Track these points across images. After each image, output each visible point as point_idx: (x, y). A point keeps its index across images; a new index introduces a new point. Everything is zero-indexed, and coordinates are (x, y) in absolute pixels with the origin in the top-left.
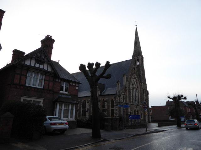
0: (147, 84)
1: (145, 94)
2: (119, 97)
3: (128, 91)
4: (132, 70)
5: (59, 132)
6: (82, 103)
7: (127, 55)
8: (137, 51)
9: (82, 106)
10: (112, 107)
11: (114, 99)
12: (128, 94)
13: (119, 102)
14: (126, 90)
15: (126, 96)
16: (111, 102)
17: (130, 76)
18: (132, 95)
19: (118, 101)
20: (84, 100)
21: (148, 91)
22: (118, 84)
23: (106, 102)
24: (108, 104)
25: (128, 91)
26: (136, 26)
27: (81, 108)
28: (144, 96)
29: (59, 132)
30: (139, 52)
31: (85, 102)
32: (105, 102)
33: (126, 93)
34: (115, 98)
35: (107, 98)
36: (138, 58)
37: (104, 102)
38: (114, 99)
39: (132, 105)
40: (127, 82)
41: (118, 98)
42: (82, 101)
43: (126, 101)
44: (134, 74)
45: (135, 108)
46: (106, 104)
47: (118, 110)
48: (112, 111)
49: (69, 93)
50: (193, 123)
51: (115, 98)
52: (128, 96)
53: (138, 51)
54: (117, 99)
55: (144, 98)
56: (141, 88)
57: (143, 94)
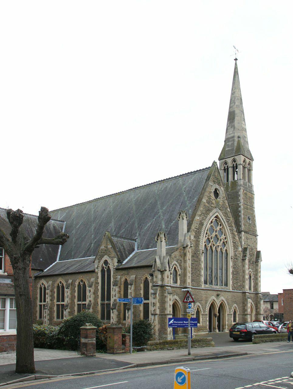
0: (259, 232)
1: (247, 261)
2: (162, 272)
3: (189, 256)
4: (209, 198)
5: (193, 325)
6: (76, 289)
7: (205, 154)
8: (234, 140)
9: (76, 294)
10: (147, 298)
11: (149, 278)
12: (189, 263)
13: (162, 286)
14: (185, 255)
15: (185, 269)
16: (142, 285)
17: (200, 215)
18: (203, 265)
19: (160, 283)
20: (82, 281)
21: (259, 252)
22: (159, 240)
23: (131, 285)
24: (137, 289)
25: (189, 256)
26: (236, 60)
27: (76, 300)
28: (244, 266)
29: (193, 325)
30: (239, 142)
31: (63, 287)
32: (129, 286)
33: (185, 261)
34: (152, 275)
35: (134, 276)
36: (234, 161)
37: (126, 284)
38: (149, 278)
39: (203, 292)
40: (188, 231)
41: (159, 276)
42: (77, 283)
43: (184, 281)
44: (215, 210)
45: (214, 297)
46: (131, 290)
47: (158, 305)
48: (146, 306)
49: (5, 272)
50: (192, 368)
51: (152, 275)
52: (189, 269)
53: (236, 139)
54: (156, 277)
55: (244, 272)
56: (235, 247)
57: (244, 260)
